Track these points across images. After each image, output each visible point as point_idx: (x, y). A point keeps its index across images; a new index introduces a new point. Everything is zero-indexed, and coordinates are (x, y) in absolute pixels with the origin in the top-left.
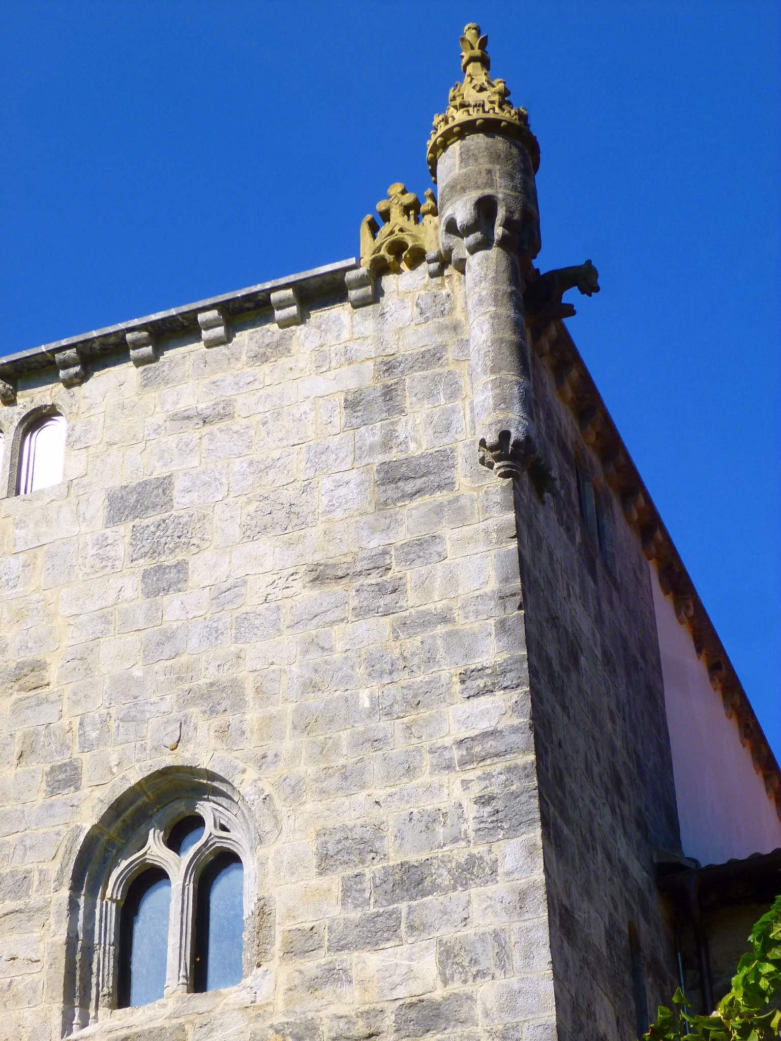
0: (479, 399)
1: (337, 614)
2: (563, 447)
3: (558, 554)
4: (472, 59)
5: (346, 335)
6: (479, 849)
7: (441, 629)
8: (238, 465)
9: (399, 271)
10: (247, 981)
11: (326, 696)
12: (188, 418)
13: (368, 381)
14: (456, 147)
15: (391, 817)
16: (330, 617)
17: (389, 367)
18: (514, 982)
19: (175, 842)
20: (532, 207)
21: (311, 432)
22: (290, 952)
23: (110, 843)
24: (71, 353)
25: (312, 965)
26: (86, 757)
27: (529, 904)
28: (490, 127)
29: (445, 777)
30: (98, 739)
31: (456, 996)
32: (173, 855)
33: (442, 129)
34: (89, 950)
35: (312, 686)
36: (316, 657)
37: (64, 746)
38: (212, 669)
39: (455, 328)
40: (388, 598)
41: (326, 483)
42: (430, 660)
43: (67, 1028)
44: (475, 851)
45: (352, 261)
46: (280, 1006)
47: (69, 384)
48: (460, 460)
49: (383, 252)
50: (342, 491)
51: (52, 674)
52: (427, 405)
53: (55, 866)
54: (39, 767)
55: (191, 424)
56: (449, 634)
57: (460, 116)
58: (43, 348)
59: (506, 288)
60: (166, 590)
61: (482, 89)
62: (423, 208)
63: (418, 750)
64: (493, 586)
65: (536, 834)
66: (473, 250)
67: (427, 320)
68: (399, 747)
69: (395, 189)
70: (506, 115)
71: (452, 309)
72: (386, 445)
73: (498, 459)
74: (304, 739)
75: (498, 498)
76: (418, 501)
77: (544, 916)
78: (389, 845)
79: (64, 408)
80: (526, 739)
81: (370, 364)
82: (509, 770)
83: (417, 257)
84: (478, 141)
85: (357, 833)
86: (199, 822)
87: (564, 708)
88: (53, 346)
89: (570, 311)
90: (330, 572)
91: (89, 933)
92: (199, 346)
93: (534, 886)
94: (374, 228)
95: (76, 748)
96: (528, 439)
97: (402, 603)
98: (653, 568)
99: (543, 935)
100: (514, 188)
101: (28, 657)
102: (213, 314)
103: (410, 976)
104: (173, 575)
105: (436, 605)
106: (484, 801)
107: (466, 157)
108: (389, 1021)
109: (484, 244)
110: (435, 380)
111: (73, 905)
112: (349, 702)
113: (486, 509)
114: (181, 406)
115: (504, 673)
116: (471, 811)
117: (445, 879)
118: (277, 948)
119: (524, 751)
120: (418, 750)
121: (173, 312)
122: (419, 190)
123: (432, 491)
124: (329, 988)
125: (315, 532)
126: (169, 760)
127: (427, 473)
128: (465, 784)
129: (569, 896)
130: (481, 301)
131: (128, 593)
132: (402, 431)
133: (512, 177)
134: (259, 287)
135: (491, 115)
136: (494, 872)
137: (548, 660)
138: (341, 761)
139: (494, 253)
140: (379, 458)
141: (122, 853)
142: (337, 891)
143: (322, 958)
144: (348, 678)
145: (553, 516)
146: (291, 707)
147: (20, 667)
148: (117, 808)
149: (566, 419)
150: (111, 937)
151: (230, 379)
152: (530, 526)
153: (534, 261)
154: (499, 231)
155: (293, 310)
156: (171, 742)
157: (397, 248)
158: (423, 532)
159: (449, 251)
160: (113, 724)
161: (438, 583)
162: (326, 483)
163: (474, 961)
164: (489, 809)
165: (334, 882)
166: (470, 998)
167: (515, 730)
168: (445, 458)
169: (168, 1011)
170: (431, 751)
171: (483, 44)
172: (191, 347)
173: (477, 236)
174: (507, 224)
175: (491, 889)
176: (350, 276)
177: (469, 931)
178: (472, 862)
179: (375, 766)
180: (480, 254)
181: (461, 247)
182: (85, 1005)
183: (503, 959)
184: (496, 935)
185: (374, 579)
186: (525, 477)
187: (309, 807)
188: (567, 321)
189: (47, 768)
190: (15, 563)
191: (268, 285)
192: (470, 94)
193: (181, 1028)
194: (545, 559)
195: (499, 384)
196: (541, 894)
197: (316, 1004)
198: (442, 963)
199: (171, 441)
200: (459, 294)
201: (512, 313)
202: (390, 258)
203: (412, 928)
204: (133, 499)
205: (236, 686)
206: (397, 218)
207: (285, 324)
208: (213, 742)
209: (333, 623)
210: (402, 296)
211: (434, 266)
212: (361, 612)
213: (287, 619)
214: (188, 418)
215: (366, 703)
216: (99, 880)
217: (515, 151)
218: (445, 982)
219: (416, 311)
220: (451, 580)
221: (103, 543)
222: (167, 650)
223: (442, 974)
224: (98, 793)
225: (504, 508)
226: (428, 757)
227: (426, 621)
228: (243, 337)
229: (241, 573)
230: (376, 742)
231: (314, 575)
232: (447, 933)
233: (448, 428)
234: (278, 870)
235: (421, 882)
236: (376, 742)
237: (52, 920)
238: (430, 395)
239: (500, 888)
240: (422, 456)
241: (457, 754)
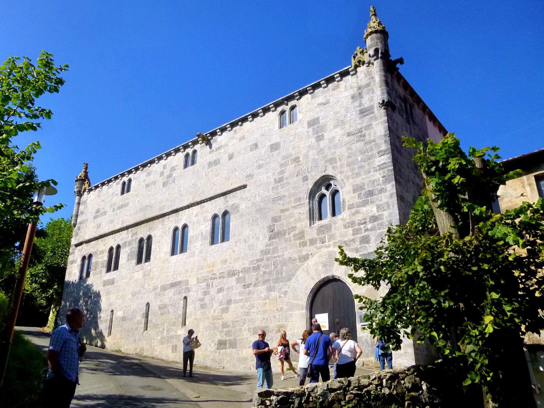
0: (378, 93)
1: (353, 142)
2: (400, 97)
3: (399, 122)
4: (372, 15)
5: (350, 82)
6: (383, 186)
7: (373, 143)
8: (331, 113)
9: (360, 66)
10: (342, 214)
11: (352, 159)
13: (356, 92)
14: (369, 37)
15: (366, 181)
16: (352, 143)
17: (359, 88)
18: (391, 211)
19: (327, 189)
20: (387, 49)
21: (345, 104)
22: (349, 208)
23: (315, 190)
24: (297, 94)
25: (353, 211)
26: (309, 174)
27: (393, 196)
28: (376, 32)
29: (376, 173)
30: (311, 171)
31: (380, 215)
33: (366, 34)
34: (313, 210)
36: (349, 151)
38: (330, 155)
39: (373, 78)
40: (363, 138)
41: (349, 115)
43: (310, 225)
44: (382, 187)
45: (350, 66)
46: (348, 218)
47: (298, 100)
48: (375, 107)
49: (357, 63)
50: (352, 116)
51: (301, 159)
52: (368, 96)
53: (306, 195)
54: (301, 177)
55: (321, 105)
56: (375, 144)
57: (370, 30)
58: (292, 93)
59: (382, 68)
60: (320, 140)
61: (374, 22)
62: (364, 52)
63: (370, 168)
64: (383, 133)
65: (394, 183)
66: (375, 60)
68: (366, 168)
69: (358, 48)
70: (379, 28)
71: (372, 74)
72: (360, 106)
73: (382, 106)
74: (348, 168)
75: (383, 114)
76: (367, 117)
77: (396, 198)
78: (366, 187)
79: (297, 105)
80: (391, 164)
82: (388, 170)
83: (364, 63)
84: (374, 35)
85: (360, 185)
86: (331, 185)
87: (401, 155)
88: (293, 93)
89: (398, 69)
90: (351, 134)
91: (313, 207)
92: (321, 89)
93: (394, 193)
94: (354, 57)
96: (389, 101)
97: (366, 139)
98: (427, 118)
99: (396, 202)
100: (382, 45)
101: (296, 156)
102: (323, 82)
103: (371, 211)
104: (321, 137)
105: (372, 138)
106: (383, 177)
107: (372, 39)
108: (368, 220)
110: (369, 90)
111: (309, 203)
112: (357, 159)
113: (381, 117)
114: (319, 102)
116: (381, 179)
117: (377, 193)
118: (347, 208)
119: (391, 166)
120: (370, 168)
121: (316, 82)
122: (363, 47)
123: (370, 114)
124: (356, 215)
125: (347, 126)
126: (324, 174)
127: (369, 110)
128: (380, 174)
129: (402, 193)
131: (313, 142)
132: (363, 102)
133: (382, 42)
134: (332, 75)
135: (376, 29)
136: (386, 190)
137: (397, 146)
138: (356, 172)
139: (379, 60)
140: (359, 108)
141: (317, 192)
142: (357, 196)
143: (355, 209)
144: (356, 155)
145: (398, 114)
146: (346, 161)
147: (295, 158)
148: (316, 184)
149: (401, 91)
150: (317, 207)
151: (328, 95)
152: (391, 119)
153: (390, 58)
154: (380, 55)
155: (339, 78)
156: (324, 170)
157: (359, 62)
158: (369, 123)
159: (370, 61)
160: (313, 168)
161: (372, 134)
162: (349, 115)
163: (383, 208)
164: (384, 178)
165: (356, 195)
166: (383, 215)
167: (389, 162)
168: (372, 107)
169: (328, 221)
170: (373, 168)
171: (375, 11)
172: (320, 89)
173: (375, 57)
174: (382, 53)
175: (386, 194)
176: (350, 69)
177: (382, 202)
178: (382, 189)
179: (363, 172)
180: (376, 61)
181: (372, 60)
182: (313, 220)
183: (388, 207)
184: (387, 203)
185: (359, 134)
186: (390, 108)
187: (350, 181)
188: (399, 70)
190: (292, 138)
191: (334, 74)
192: (372, 24)
193: (330, 224)
194: (395, 124)
195: (382, 90)
196: (395, 194)
197: (354, 218)
198: (377, 208)
199: (318, 109)
200: (373, 70)
201: (384, 73)
202: (358, 64)
203: (371, 202)
204: (312, 123)
205: (335, 158)
206: (359, 55)
207: (338, 81)
208: (332, 170)
209: (352, 144)
210: (361, 72)
211: (367, 65)
212: (358, 141)
213: (344, 144)
215: (360, 159)
216: (314, 197)
217: (382, 36)
218: (378, 212)
220: (375, 133)
221: (307, 132)
222: (322, 152)
223: (377, 211)
224: (312, 181)
225: (385, 116)
226: (372, 169)
227: (370, 142)
228: (330, 85)
229: (333, 136)
232: (378, 203)
233: (372, 100)
234: (346, 193)
235: (372, 193)
237: (306, 206)
238: (368, 93)
239: (387, 194)
241: (378, 168)
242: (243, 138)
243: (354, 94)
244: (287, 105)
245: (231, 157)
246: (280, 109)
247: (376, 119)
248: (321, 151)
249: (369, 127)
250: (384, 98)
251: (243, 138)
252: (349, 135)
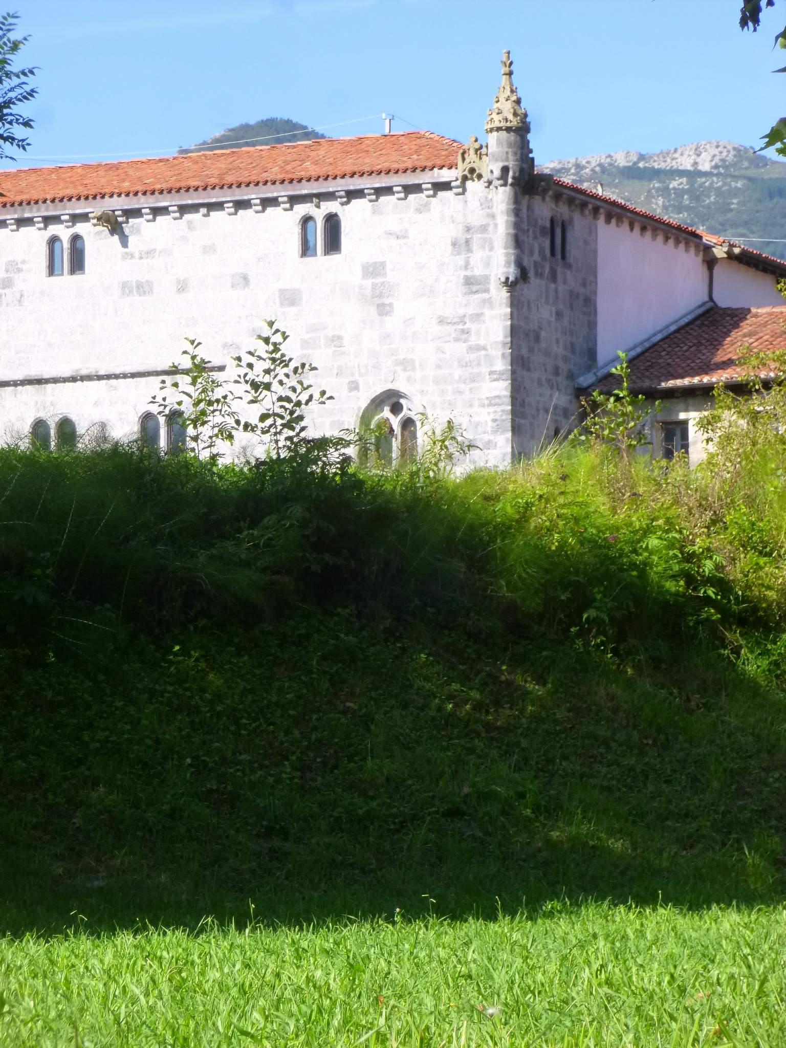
6: (492, 437)
7: (483, 353)
12: (390, 234)
17: (468, 229)
32: (375, 391)
35: (439, 367)
37: (353, 374)
42: (479, 364)
47: (342, 204)
51: (346, 342)
56: (487, 355)
65: (509, 435)
67: (483, 209)
71: (492, 207)
80: (508, 400)
81: (461, 225)
95: (357, 375)
101: (337, 333)
105: (482, 342)
106: (495, 420)
109: (505, 185)
115: (503, 374)
116: (490, 424)
119: (508, 405)
128: (489, 413)
130: (502, 212)
136: (496, 446)
138: (449, 398)
147: (334, 336)
148: (373, 401)
154: (510, 180)
167: (505, 396)
168: (486, 278)
174: (514, 178)
178: (489, 442)
180: (503, 188)
185: (460, 327)
189: (347, 381)
195: (507, 255)
204: (371, 269)
209: (446, 342)
212: (457, 340)
214: (390, 234)
219: (479, 204)
225: (507, 306)
230: (460, 393)
231: (439, 320)
236: (460, 393)
240: (480, 276)
241: (486, 402)
242: (209, 250)
243: (456, 239)
244: (318, 206)
245: (182, 287)
246: (302, 209)
247: (489, 302)
248: (386, 337)
249: (477, 317)
250: (508, 273)
251: (209, 250)
252: (442, 321)
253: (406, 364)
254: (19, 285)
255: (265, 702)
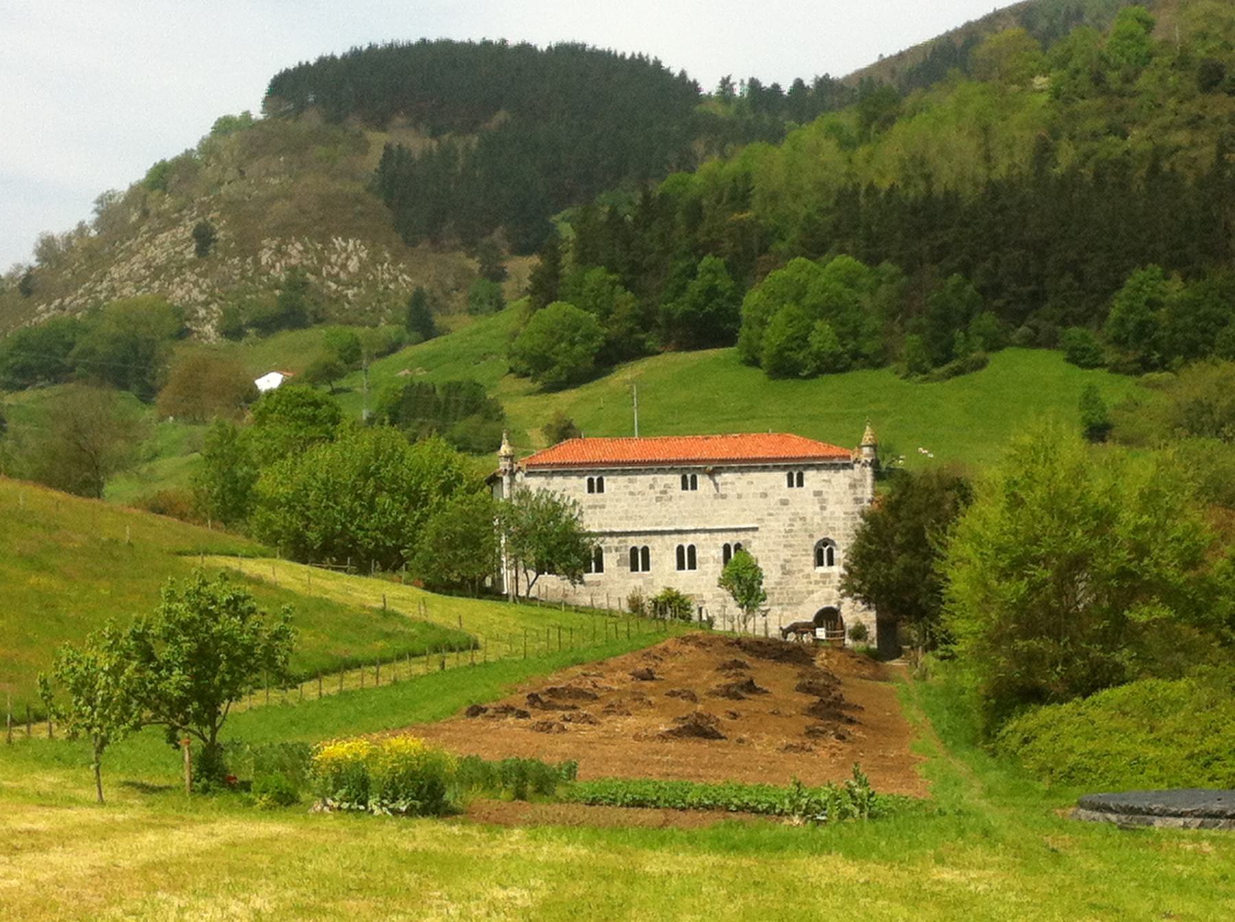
245: (739, 496)
248: (823, 518)
253: (833, 529)
254: (670, 494)
255: (1044, 681)
